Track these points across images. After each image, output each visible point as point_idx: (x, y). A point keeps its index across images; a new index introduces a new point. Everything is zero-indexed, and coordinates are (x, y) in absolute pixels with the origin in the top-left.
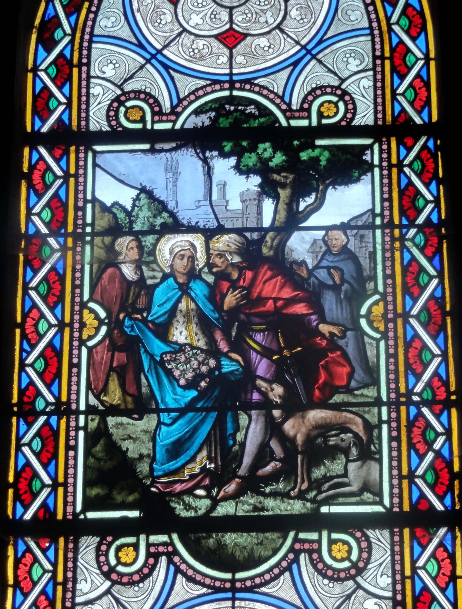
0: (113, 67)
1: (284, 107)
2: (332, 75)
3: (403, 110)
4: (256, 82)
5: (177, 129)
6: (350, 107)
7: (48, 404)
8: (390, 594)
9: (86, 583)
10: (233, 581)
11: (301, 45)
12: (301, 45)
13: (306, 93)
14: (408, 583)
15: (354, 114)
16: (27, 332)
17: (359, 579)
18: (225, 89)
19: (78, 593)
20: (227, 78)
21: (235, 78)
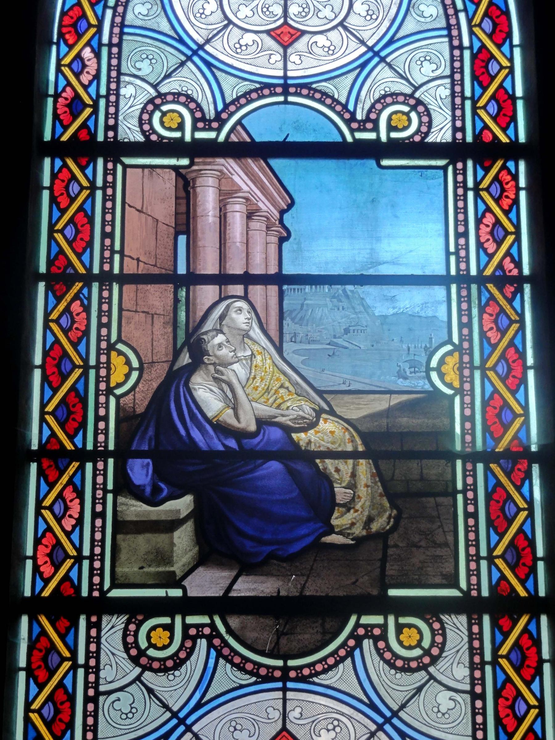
0: (440, 707)
1: (217, 642)
6: (130, 639)
8: (468, 688)
11: (366, 46)
12: (366, 46)
14: (103, 91)
15: (126, 629)
17: (431, 669)
20: (281, 81)
21: (290, 82)
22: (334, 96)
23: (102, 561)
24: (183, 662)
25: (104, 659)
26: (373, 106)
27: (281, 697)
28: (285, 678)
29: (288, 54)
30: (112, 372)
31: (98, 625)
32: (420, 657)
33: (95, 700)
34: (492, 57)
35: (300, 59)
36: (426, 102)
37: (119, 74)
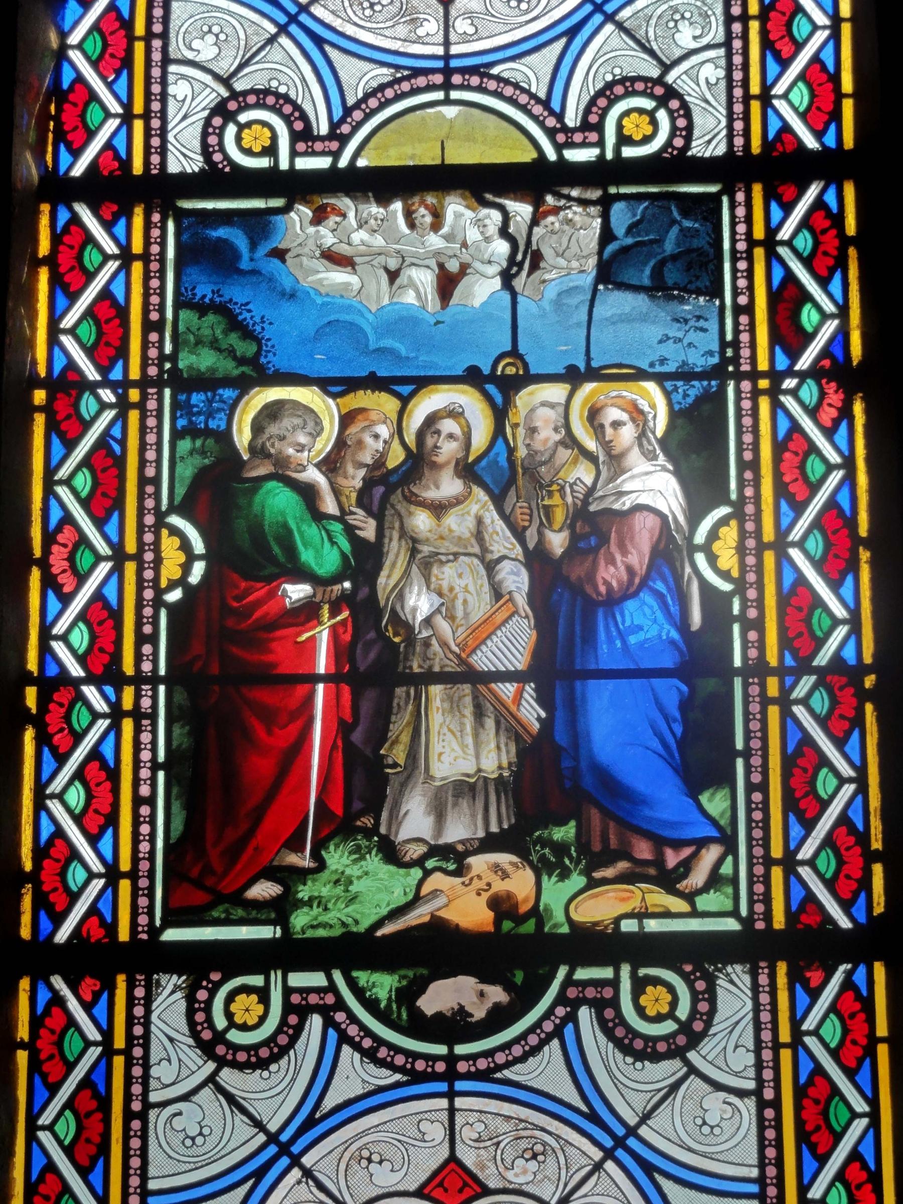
1: (551, 122)
2: (646, 57)
3: (786, 128)
4: (495, 71)
7: (794, 392)
8: (751, 1085)
9: (707, 79)
10: (451, 1059)
13: (592, 93)
15: (688, 139)
16: (55, 570)
17: (692, 1055)
19: (153, 1084)
28: (451, 1075)
29: (446, 1145)
32: (673, 1035)
33: (143, 1116)
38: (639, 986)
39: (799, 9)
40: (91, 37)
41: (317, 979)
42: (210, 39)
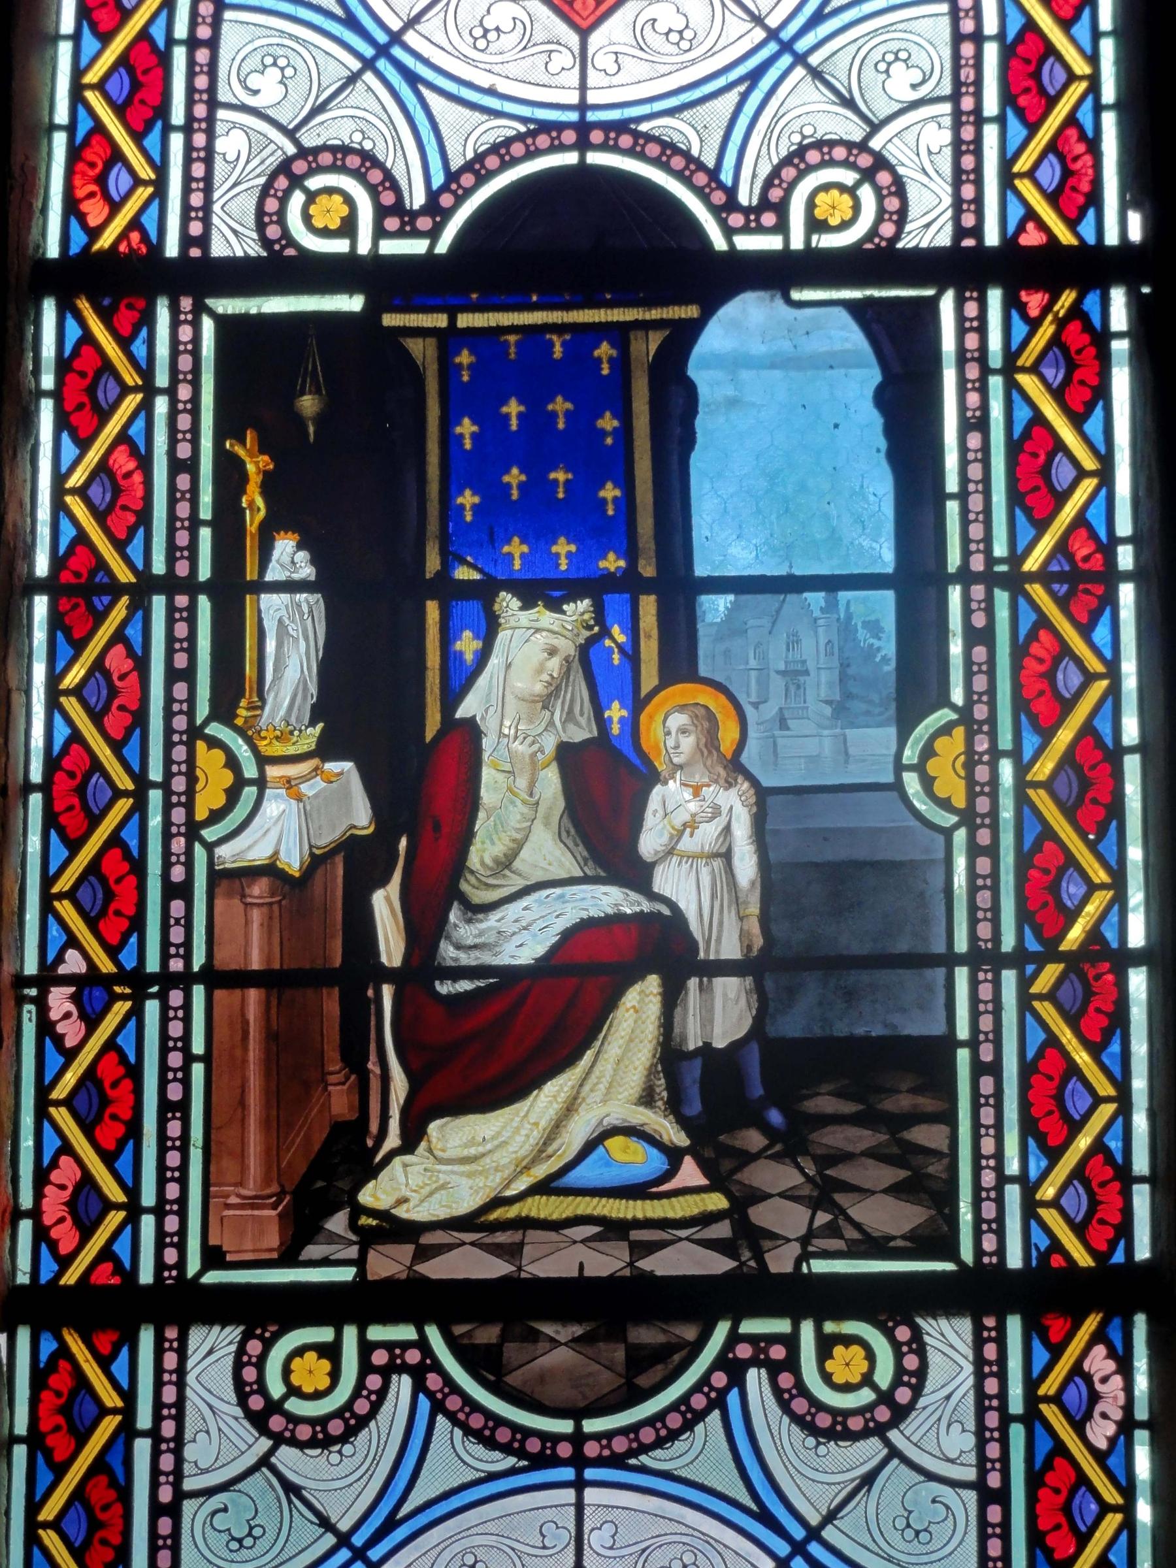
5: (440, 255)
8: (971, 1474)
10: (578, 1438)
11: (766, 27)
12: (766, 27)
13: (372, 1424)
15: (241, 1351)
17: (291, 150)
18: (597, 1437)
22: (689, 150)
23: (183, 1215)
24: (363, 1422)
25: (947, 168)
26: (776, 172)
27: (573, 1501)
29: (591, 51)
30: (199, 787)
31: (960, 232)
32: (870, 1408)
33: (173, 1511)
34: (1050, 50)
35: (616, 61)
36: (894, 161)
37: (213, 104)
38: (826, 1346)
39: (77, 1554)
40: (116, 75)
41: (746, 243)
42: (274, 74)
